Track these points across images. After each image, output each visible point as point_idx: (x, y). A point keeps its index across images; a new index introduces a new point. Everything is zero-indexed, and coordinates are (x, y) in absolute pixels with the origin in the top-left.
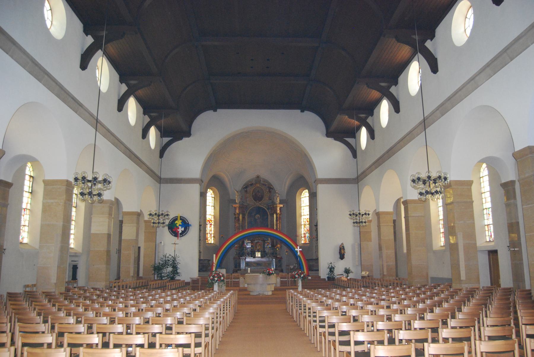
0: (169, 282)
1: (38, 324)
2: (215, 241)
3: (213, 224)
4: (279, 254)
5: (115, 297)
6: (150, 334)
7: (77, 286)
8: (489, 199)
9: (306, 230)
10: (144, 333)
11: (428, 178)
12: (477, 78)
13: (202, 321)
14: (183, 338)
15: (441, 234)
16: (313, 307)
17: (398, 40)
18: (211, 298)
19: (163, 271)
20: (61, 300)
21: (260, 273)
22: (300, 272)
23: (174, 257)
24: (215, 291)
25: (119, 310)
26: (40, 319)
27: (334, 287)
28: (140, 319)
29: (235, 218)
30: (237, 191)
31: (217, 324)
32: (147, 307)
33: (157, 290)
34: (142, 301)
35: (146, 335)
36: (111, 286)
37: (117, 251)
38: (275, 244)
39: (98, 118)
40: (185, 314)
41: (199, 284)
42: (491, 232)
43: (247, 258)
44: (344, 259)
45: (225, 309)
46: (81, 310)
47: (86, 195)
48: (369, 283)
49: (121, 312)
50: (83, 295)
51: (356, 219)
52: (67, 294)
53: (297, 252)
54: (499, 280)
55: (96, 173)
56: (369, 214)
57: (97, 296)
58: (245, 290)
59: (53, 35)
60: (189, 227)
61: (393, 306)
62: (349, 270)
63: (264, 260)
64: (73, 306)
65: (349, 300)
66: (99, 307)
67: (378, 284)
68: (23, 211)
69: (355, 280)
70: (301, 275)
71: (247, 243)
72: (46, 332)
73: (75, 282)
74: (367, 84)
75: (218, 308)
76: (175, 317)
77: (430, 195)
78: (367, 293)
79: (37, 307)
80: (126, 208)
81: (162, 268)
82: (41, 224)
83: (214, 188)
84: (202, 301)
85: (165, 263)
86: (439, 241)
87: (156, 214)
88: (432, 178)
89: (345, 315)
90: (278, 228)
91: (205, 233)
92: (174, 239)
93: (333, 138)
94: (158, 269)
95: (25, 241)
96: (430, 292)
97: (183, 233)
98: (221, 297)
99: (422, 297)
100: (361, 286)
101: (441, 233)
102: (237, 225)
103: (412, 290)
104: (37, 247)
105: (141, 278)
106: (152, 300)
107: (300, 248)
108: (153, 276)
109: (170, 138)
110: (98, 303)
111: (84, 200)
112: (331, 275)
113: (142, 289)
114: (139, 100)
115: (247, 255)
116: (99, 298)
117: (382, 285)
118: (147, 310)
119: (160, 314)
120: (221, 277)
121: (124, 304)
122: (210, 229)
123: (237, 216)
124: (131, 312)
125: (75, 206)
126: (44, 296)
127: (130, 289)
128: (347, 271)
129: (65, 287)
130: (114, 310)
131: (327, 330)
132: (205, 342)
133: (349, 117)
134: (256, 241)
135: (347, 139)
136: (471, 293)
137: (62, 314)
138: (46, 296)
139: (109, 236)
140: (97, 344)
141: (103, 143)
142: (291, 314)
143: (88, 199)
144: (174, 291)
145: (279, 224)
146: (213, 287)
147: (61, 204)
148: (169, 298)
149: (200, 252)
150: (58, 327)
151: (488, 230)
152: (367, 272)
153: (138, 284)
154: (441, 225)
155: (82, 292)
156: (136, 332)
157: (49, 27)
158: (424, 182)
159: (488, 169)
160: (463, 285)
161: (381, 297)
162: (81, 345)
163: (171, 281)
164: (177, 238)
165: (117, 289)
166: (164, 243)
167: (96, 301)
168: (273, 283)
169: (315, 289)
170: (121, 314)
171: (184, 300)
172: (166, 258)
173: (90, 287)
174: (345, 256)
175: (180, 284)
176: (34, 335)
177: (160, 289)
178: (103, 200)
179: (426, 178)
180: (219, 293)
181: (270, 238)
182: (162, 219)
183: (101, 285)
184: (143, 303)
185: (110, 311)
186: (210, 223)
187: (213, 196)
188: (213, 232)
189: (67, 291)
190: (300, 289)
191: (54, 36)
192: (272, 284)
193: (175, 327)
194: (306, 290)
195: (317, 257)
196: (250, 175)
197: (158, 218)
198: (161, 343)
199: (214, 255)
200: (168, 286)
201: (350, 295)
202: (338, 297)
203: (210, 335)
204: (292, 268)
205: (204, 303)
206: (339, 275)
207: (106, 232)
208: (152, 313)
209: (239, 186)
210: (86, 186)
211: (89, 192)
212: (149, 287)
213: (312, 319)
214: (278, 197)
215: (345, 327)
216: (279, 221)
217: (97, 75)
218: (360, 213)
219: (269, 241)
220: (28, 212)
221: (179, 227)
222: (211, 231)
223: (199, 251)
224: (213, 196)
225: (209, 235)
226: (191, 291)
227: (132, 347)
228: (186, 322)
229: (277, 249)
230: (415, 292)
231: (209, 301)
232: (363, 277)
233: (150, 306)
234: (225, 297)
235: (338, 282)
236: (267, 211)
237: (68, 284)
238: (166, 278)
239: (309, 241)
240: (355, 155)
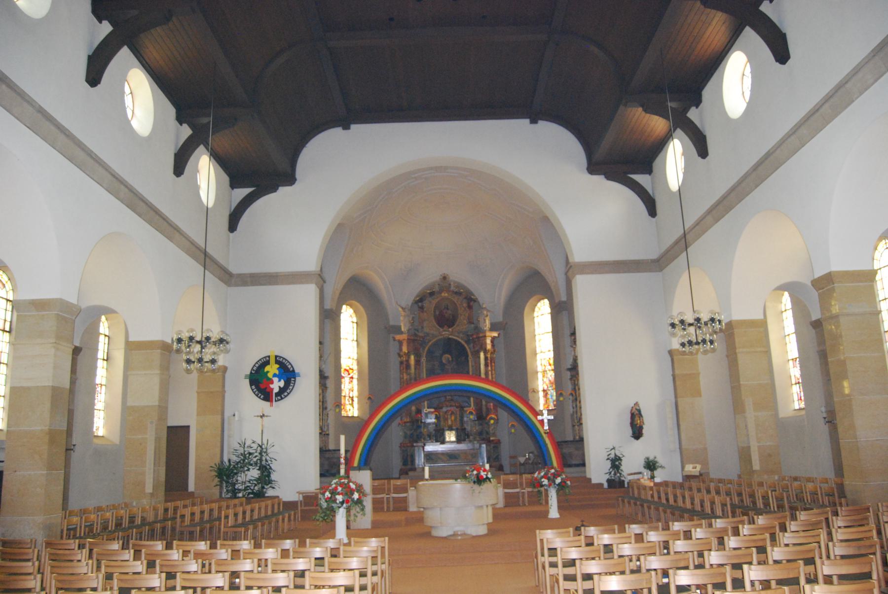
3: (356, 376)
6: (270, 589)
9: (547, 382)
29: (401, 363)
30: (402, 308)
38: (484, 414)
39: (207, 250)
60: (295, 378)
62: (656, 462)
63: (463, 446)
70: (556, 478)
71: (426, 414)
83: (354, 302)
97: (283, 393)
102: (405, 378)
109: (247, 191)
115: (428, 439)
120: (352, 492)
123: (404, 359)
128: (651, 464)
145: (492, 372)
157: (130, 119)
174: (644, 431)
186: (349, 374)
188: (355, 394)
191: (137, 132)
196: (428, 277)
204: (522, 462)
206: (632, 474)
209: (409, 296)
214: (487, 316)
216: (491, 366)
219: (473, 407)
222: (352, 391)
229: (492, 422)
232: (688, 478)
236: (466, 346)
239: (555, 406)
240: (652, 212)
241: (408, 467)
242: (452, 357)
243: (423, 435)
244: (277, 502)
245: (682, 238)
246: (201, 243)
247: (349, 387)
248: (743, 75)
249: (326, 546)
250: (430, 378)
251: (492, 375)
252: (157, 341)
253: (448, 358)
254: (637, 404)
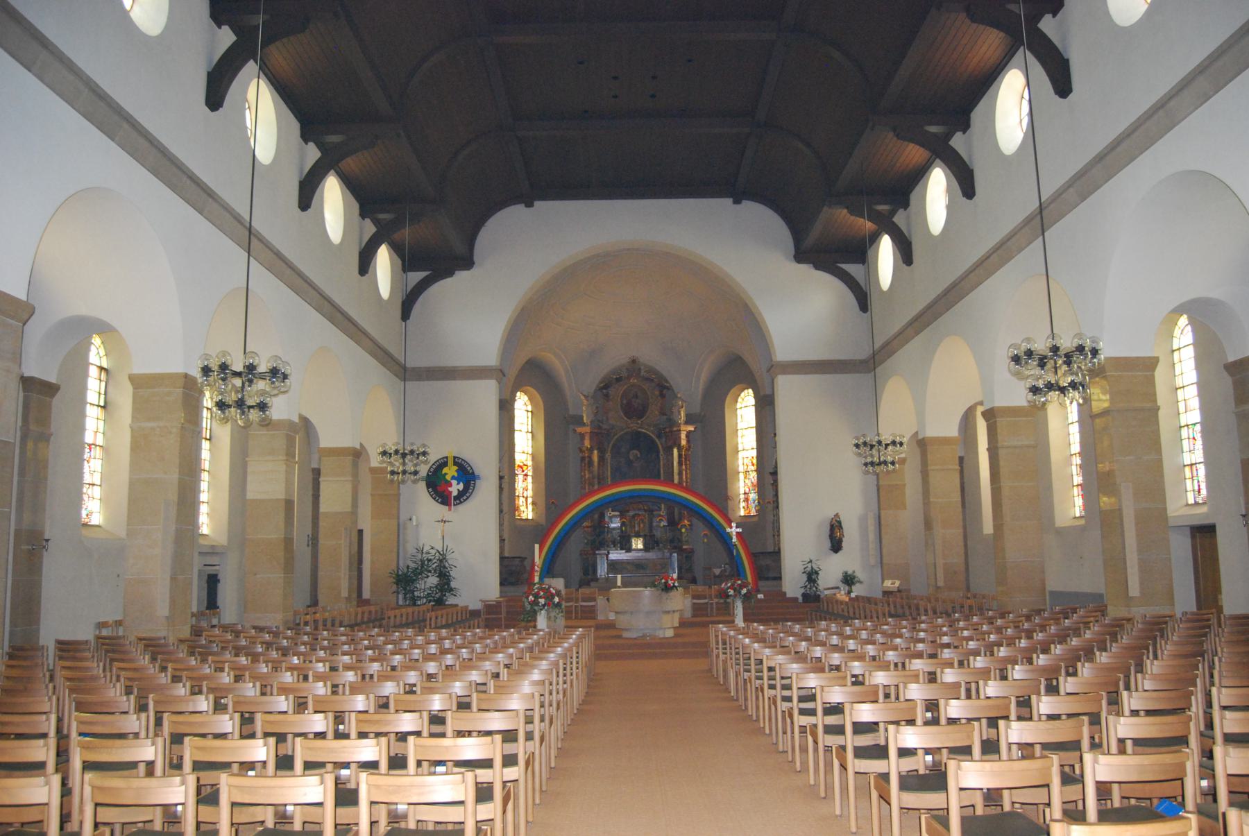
0: (432, 611)
1: (124, 716)
2: (536, 513)
3: (530, 473)
4: (686, 542)
5: (306, 648)
6: (392, 736)
7: (219, 622)
8: (1195, 403)
9: (750, 484)
10: (378, 735)
11: (1051, 352)
12: (1172, 103)
13: (515, 703)
14: (474, 745)
15: (1075, 488)
16: (780, 664)
17: (973, 18)
18: (533, 647)
19: (418, 586)
20: (181, 655)
21: (646, 587)
22: (739, 582)
23: (442, 553)
24: (540, 630)
25: (316, 677)
26: (130, 703)
27: (818, 618)
28: (368, 698)
29: (583, 459)
30: (584, 396)
31: (551, 708)
32: (383, 671)
33: (405, 630)
34: (369, 656)
35: (383, 740)
36: (298, 622)
37: (308, 541)
39: (253, 224)
40: (474, 686)
41: (501, 614)
42: (1198, 482)
43: (611, 552)
44: (840, 552)
45: (568, 672)
46: (226, 678)
47: (229, 406)
48: (903, 607)
49: (321, 684)
50: (231, 644)
51: (872, 456)
52: (197, 643)
53: (729, 536)
54: (1219, 597)
55: (253, 355)
56: (901, 444)
57: (264, 646)
58: (611, 625)
59: (137, 24)
60: (474, 481)
61: (975, 660)
62: (854, 577)
63: (651, 555)
64: (208, 671)
65: (864, 647)
66: (270, 671)
67: (926, 611)
68: (87, 450)
69: (868, 600)
71: (611, 518)
72: (143, 734)
73: (214, 615)
74: (894, 130)
75: (552, 670)
76: (450, 694)
77: (1057, 393)
78: (904, 630)
79: (124, 673)
80: (329, 438)
81: (414, 578)
82: (130, 479)
84: (512, 654)
85: (422, 567)
86: (1071, 505)
87: (396, 452)
88: (1062, 352)
89: (862, 683)
90: (685, 480)
91: (512, 496)
92: (441, 510)
93: (811, 265)
94: (405, 580)
95: (96, 519)
96: (1056, 627)
97: (462, 497)
98: (555, 643)
99: (1039, 638)
100: (884, 615)
101: (1073, 486)
102: (587, 476)
103: (1011, 622)
104: (123, 534)
105: (367, 602)
106: (393, 653)
107: (737, 527)
108: (393, 598)
109: (423, 274)
110: (266, 662)
111: (225, 420)
112: (810, 589)
113: (369, 627)
114: (348, 182)
115: (612, 546)
116: (270, 649)
117: (935, 613)
118: (384, 678)
119: (415, 685)
120: (553, 596)
121: (327, 664)
122: (525, 487)
124: (346, 681)
125: (208, 437)
126: (141, 646)
127: (342, 629)
128: (849, 578)
129: (190, 626)
130: (306, 678)
131: (820, 720)
132: (526, 753)
133: (852, 212)
134: (631, 513)
135: (844, 266)
136: (1156, 628)
137: (181, 690)
138: (146, 646)
139: (289, 504)
140: (264, 762)
141: (265, 283)
142: (722, 683)
143: (236, 417)
144: (444, 631)
145: (686, 471)
146: (535, 620)
147: (174, 430)
148: (433, 649)
149: (502, 540)
150: (169, 721)
151: (1193, 477)
152: (897, 581)
153: (359, 616)
154: (1074, 468)
155: (230, 638)
156: (359, 733)
158: (1042, 364)
159: (1194, 331)
160: (1134, 610)
161: (940, 639)
162: (225, 766)
163: (436, 607)
164: (447, 507)
165: (311, 628)
166: (417, 520)
167: (262, 657)
168: (677, 609)
169: (776, 621)
170: (321, 689)
171: (468, 652)
172: (424, 555)
173: (248, 625)
175: (457, 616)
176: (118, 742)
177: (411, 626)
178: (271, 420)
179: (1048, 351)
180: (549, 634)
181: (665, 505)
182: (410, 464)
183: (274, 619)
184: (373, 660)
185: (296, 681)
186: (523, 471)
187: (530, 410)
188: (530, 493)
189: (197, 636)
190: (740, 622)
191: (141, 28)
192: (674, 611)
193: (452, 718)
194: (755, 624)
195: (777, 548)
196: (615, 358)
197: (401, 461)
198: (419, 758)
199: (537, 546)
200: (431, 619)
201: (864, 634)
202: (835, 640)
203: (537, 736)
205: (517, 658)
206: (829, 589)
207: (282, 496)
208: (394, 684)
209: (591, 382)
210: (230, 386)
211: (237, 399)
212: (384, 622)
213: (779, 693)
215: (866, 713)
216: (686, 465)
217: (248, 124)
218: (879, 441)
219: (663, 512)
220: (97, 452)
221: (452, 481)
223: (500, 537)
224: (530, 410)
225: (521, 499)
226: (483, 630)
227: (349, 768)
228: (478, 705)
229: (683, 530)
230: (1019, 627)
231: (528, 654)
232: (887, 593)
233: (389, 668)
234: (566, 645)
235: (828, 606)
236: (657, 440)
237: (198, 620)
238: (425, 600)
241: (588, 575)
242: (641, 454)
243: (607, 541)
244: (440, 615)
245: (1036, 215)
247: (523, 486)
248: (1023, 97)
249: (450, 692)
250: (614, 485)
251: (686, 474)
252: (349, 448)
253: (636, 455)
254: (837, 515)
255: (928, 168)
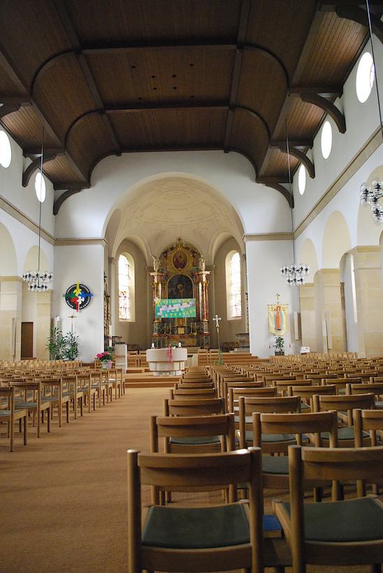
17: (341, 15)
97: (84, 305)
107: (218, 317)
188: (128, 306)
196: (169, 240)
209: (158, 251)
246: (38, 224)
255: (322, 123)
